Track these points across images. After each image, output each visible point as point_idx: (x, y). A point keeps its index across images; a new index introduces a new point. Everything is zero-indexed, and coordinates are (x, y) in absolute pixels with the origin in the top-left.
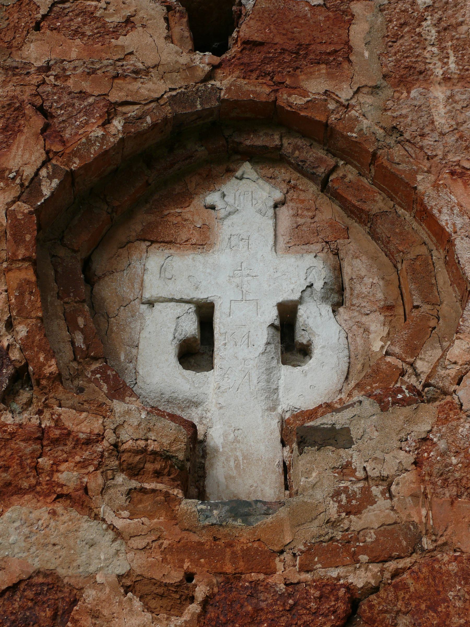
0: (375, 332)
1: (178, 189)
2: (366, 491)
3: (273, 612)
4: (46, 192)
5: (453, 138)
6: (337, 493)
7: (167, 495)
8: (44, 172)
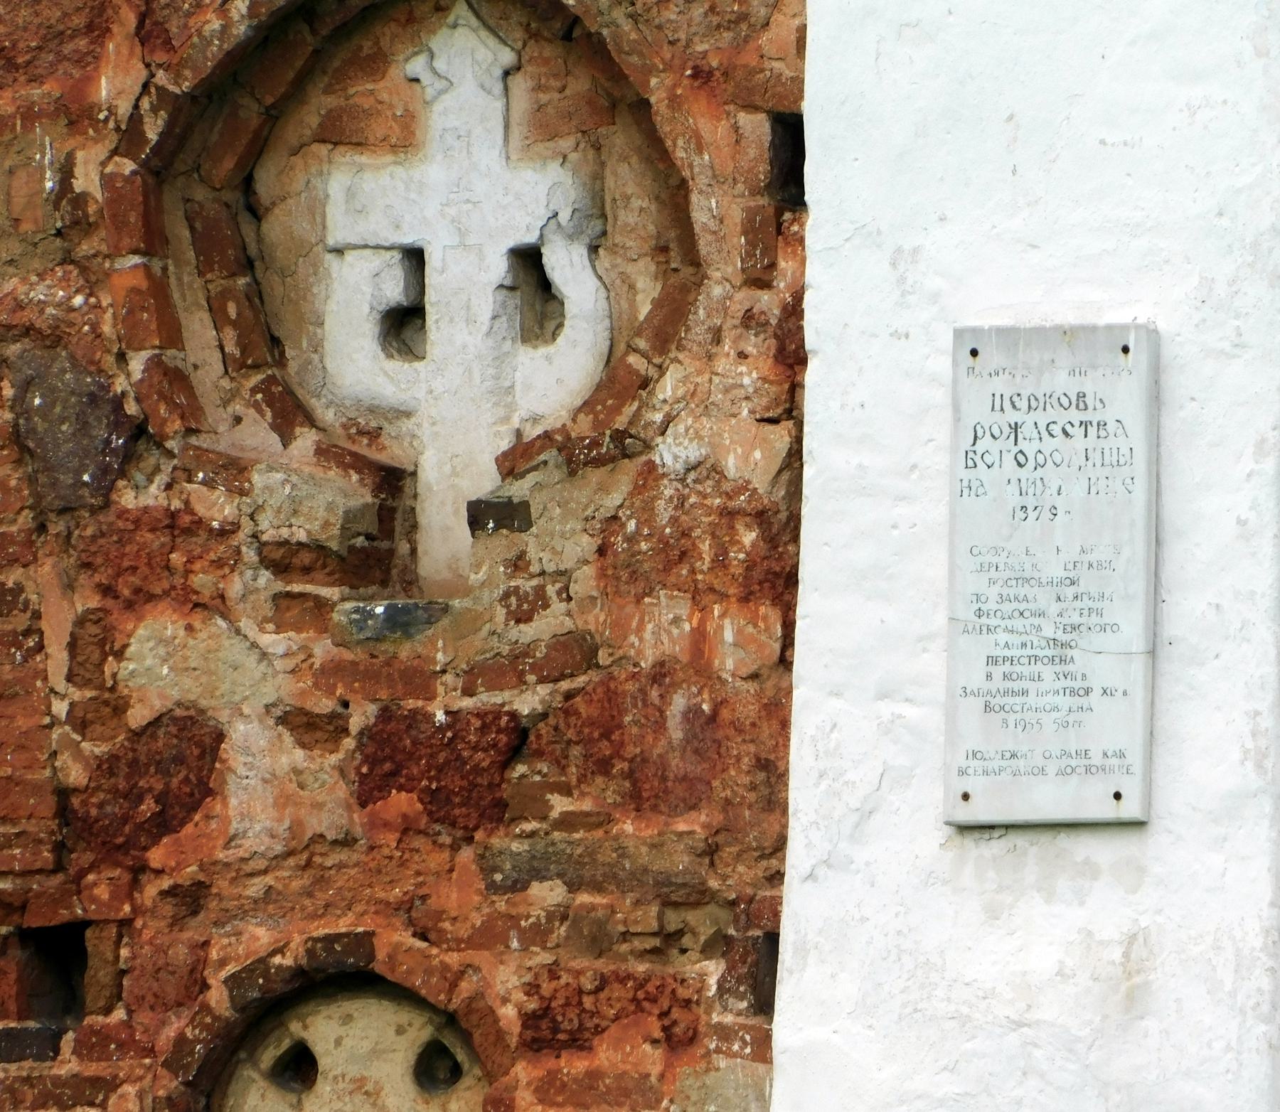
0: (644, 291)
1: (367, 47)
2: (540, 592)
3: (431, 746)
4: (152, 135)
5: (701, 10)
6: (506, 595)
7: (317, 598)
8: (145, 104)
